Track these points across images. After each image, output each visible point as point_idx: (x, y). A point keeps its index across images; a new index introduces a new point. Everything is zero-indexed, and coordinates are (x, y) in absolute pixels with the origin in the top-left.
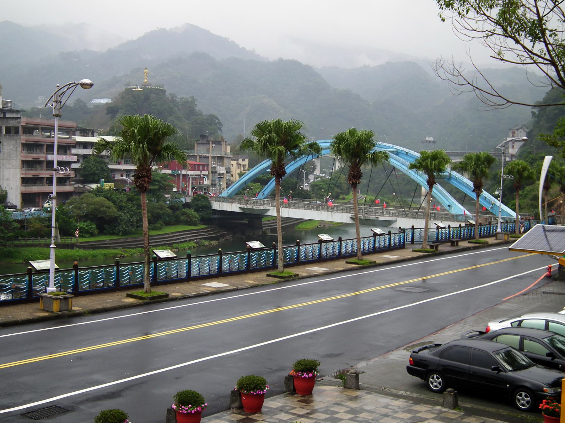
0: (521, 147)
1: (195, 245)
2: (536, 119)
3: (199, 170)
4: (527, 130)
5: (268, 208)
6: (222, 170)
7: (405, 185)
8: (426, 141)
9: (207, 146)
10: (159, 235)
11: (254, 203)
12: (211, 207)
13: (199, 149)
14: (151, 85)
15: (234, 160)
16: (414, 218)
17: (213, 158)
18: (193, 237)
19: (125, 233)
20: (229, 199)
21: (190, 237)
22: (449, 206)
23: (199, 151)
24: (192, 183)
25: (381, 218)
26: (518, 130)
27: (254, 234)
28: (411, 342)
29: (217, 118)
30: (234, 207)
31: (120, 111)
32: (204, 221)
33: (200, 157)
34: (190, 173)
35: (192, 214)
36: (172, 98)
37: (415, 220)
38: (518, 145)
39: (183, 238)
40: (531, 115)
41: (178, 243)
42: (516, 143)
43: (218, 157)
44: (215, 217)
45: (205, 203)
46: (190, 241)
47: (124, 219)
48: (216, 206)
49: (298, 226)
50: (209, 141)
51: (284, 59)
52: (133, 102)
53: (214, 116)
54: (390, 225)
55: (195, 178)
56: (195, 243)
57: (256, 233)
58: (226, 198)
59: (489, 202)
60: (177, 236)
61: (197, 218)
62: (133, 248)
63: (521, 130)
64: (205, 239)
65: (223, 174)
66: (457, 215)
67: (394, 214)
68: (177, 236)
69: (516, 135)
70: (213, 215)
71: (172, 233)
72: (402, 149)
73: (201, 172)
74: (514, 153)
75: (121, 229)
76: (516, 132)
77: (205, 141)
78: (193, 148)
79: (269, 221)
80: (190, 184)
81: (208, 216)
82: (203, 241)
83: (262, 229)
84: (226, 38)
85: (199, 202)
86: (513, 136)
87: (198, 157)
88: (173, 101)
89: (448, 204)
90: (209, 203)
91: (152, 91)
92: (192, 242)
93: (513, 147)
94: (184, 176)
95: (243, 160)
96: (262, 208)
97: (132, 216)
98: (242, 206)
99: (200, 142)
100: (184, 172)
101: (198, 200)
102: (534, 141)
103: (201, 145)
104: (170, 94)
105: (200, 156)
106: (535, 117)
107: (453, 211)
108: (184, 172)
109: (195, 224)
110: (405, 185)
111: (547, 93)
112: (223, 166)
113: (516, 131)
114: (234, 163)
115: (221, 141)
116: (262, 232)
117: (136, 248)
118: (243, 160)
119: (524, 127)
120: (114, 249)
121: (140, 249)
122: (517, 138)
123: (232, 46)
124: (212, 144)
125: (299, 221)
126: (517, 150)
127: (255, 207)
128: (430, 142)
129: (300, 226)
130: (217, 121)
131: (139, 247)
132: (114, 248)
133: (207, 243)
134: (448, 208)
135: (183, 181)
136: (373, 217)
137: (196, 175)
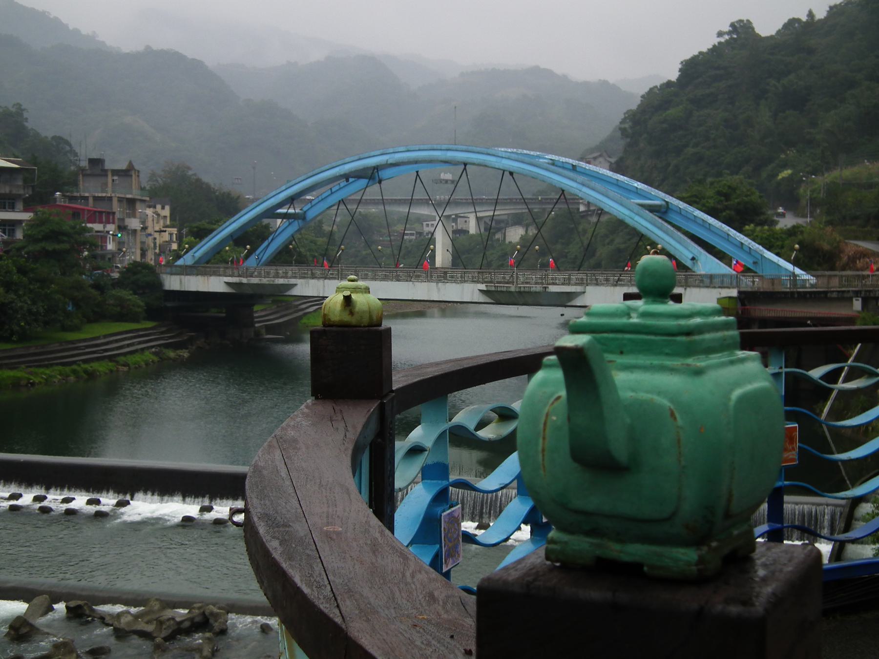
1: (156, 359)
2: (628, 140)
4: (613, 160)
5: (293, 281)
6: (134, 223)
8: (441, 181)
10: (85, 340)
12: (160, 284)
15: (150, 207)
17: (120, 200)
19: (24, 337)
20: (201, 268)
21: (140, 343)
22: (693, 259)
25: (553, 289)
29: (68, 143)
30: (216, 284)
32: (152, 313)
33: (96, 199)
35: (129, 300)
39: (128, 345)
41: (125, 354)
44: (169, 304)
46: (143, 350)
47: (21, 308)
48: (173, 283)
51: (155, 48)
53: (60, 138)
54: (570, 301)
56: (155, 354)
58: (190, 267)
59: (750, 252)
60: (117, 341)
61: (139, 306)
62: (47, 366)
63: (601, 159)
64: (167, 346)
65: (135, 231)
66: (711, 277)
68: (117, 341)
71: (105, 336)
72: (567, 160)
75: (16, 328)
83: (252, 324)
84: (44, 13)
87: (91, 200)
89: (690, 256)
92: (147, 353)
95: (163, 208)
96: (281, 281)
97: (34, 303)
109: (135, 319)
111: (643, 97)
112: (135, 217)
114: (149, 212)
117: (52, 365)
118: (163, 208)
120: (11, 369)
121: (60, 368)
123: (57, 25)
124: (113, 175)
127: (265, 281)
128: (446, 181)
129: (304, 321)
130: (68, 148)
131: (57, 364)
132: (12, 367)
133: (172, 354)
134: (689, 263)
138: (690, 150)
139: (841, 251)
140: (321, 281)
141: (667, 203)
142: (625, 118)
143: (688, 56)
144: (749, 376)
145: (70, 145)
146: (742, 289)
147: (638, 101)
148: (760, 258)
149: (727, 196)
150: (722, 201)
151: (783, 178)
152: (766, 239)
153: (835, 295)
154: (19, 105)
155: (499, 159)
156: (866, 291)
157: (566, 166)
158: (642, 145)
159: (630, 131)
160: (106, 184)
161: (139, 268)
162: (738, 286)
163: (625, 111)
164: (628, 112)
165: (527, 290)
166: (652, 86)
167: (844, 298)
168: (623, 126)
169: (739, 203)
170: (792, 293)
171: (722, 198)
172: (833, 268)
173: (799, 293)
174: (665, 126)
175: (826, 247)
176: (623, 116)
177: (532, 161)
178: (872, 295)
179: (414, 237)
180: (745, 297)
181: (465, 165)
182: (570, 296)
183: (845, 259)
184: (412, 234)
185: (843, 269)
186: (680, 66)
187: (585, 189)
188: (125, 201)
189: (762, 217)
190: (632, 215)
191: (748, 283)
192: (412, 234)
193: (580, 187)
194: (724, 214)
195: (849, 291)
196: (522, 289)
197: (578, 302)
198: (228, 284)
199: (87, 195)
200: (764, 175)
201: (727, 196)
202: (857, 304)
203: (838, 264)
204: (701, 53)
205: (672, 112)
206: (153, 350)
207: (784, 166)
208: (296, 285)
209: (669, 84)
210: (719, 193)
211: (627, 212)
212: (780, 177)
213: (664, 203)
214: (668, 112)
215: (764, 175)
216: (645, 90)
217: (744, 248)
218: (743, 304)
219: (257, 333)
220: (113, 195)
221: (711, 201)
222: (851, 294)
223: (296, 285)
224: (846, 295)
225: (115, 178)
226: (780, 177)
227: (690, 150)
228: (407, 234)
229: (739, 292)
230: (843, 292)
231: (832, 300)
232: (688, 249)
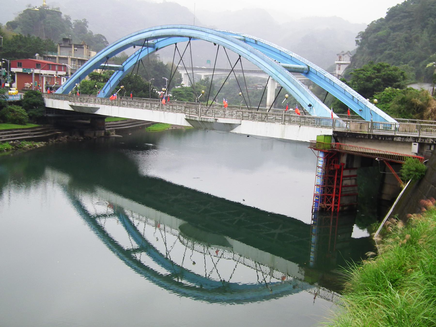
0: (346, 69)
1: (10, 147)
3: (54, 69)
4: (351, 56)
5: (97, 106)
7: (254, 98)
9: (69, 49)
11: (95, 102)
12: (44, 104)
13: (62, 52)
14: (48, 7)
16: (262, 121)
17: (72, 59)
18: (12, 137)
20: (64, 96)
22: (310, 106)
23: (62, 53)
24: (46, 82)
25: (221, 120)
26: (343, 55)
27: (95, 135)
28: (255, 72)
29: (104, 37)
30: (64, 105)
31: (18, 26)
32: (33, 119)
33: (60, 58)
34: (43, 72)
36: (67, 19)
37: (264, 123)
38: (343, 68)
40: (355, 42)
42: (341, 66)
43: (79, 60)
44: (50, 115)
45: (36, 100)
48: (51, 103)
49: (149, 127)
50: (71, 45)
52: (30, 19)
53: (101, 35)
54: (232, 129)
55: (50, 78)
57: (97, 134)
61: (25, 116)
63: (346, 55)
64: (27, 140)
66: (319, 119)
67: (237, 117)
69: (342, 59)
70: (47, 113)
73: (57, 73)
74: (340, 74)
76: (342, 57)
77: (67, 45)
78: (56, 51)
79: (117, 121)
80: (44, 83)
81: (40, 114)
82: (24, 142)
83: (104, 129)
85: (30, 98)
86: (340, 60)
87: (57, 58)
88: (68, 21)
90: (43, 100)
91: (48, 12)
93: (339, 69)
94: (37, 75)
98: (71, 103)
99: (63, 45)
100: (37, 71)
101: (30, 97)
102: (357, 64)
103: (64, 49)
104: (65, 16)
105: (59, 57)
106: (359, 44)
107: (314, 113)
108: (37, 71)
110: (254, 98)
111: (368, 26)
113: (342, 56)
115: (82, 45)
116: (105, 133)
119: (349, 53)
122: (342, 62)
124: (74, 47)
125: (150, 123)
126: (342, 71)
130: (104, 40)
133: (27, 145)
134: (307, 109)
135: (35, 80)
136: (211, 119)
137: (49, 75)
138: (387, 52)
139: (429, 106)
140: (110, 106)
141: (309, 67)
142: (359, 36)
143: (391, 7)
144: (431, 153)
145: (106, 39)
146: (337, 130)
147: (366, 27)
148: (364, 107)
149: (379, 71)
150: (374, 73)
151: (429, 67)
152: (388, 96)
153: (399, 139)
154: (85, 20)
155: (207, 34)
156: (422, 138)
157: (252, 41)
158: (364, 48)
159: (360, 42)
160: (71, 52)
161: (32, 94)
162: (333, 126)
163: (359, 32)
164: (360, 32)
165: (205, 120)
166: (373, 21)
167: (405, 141)
168: (357, 39)
169: (384, 75)
170: (369, 135)
171: (376, 71)
172: (422, 117)
173: (374, 135)
174: (376, 40)
175: (419, 102)
176: (357, 35)
177: (225, 36)
178: (426, 142)
179: (261, 89)
180: (339, 136)
181: (190, 38)
182: (231, 126)
183: (430, 111)
184: (261, 87)
185: (428, 118)
186: (388, 11)
187: (252, 55)
188: (77, 60)
189: (397, 83)
190: (277, 73)
191: (344, 125)
192: (261, 87)
193: (248, 53)
194: (375, 80)
195: (409, 137)
196: (203, 120)
197: (236, 130)
198: (71, 106)
199: (55, 56)
200: (421, 65)
201: (379, 71)
202: (415, 148)
203: (426, 114)
204: (398, 5)
205: (381, 33)
206: (12, 142)
207: (431, 61)
208: (99, 108)
209: (381, 19)
210: (374, 69)
211: (274, 71)
212: (427, 66)
213: (306, 67)
214: (379, 33)
215: (421, 65)
216: (369, 23)
217: (355, 100)
218: (336, 141)
219: (107, 134)
220: (68, 57)
221: (369, 73)
222: (411, 140)
223: (99, 108)
224: (407, 140)
225: (76, 49)
226: (427, 66)
227: (387, 52)
228: (259, 87)
229: (334, 132)
230: (405, 137)
231: (397, 142)
232: (308, 98)
